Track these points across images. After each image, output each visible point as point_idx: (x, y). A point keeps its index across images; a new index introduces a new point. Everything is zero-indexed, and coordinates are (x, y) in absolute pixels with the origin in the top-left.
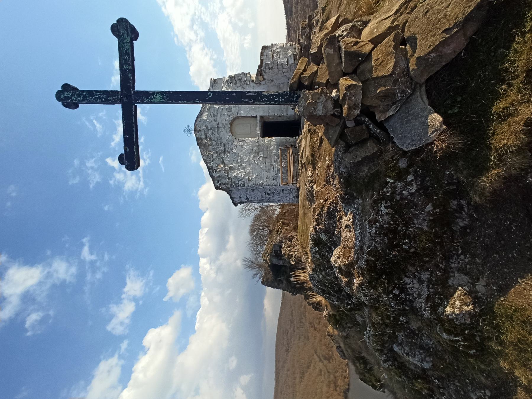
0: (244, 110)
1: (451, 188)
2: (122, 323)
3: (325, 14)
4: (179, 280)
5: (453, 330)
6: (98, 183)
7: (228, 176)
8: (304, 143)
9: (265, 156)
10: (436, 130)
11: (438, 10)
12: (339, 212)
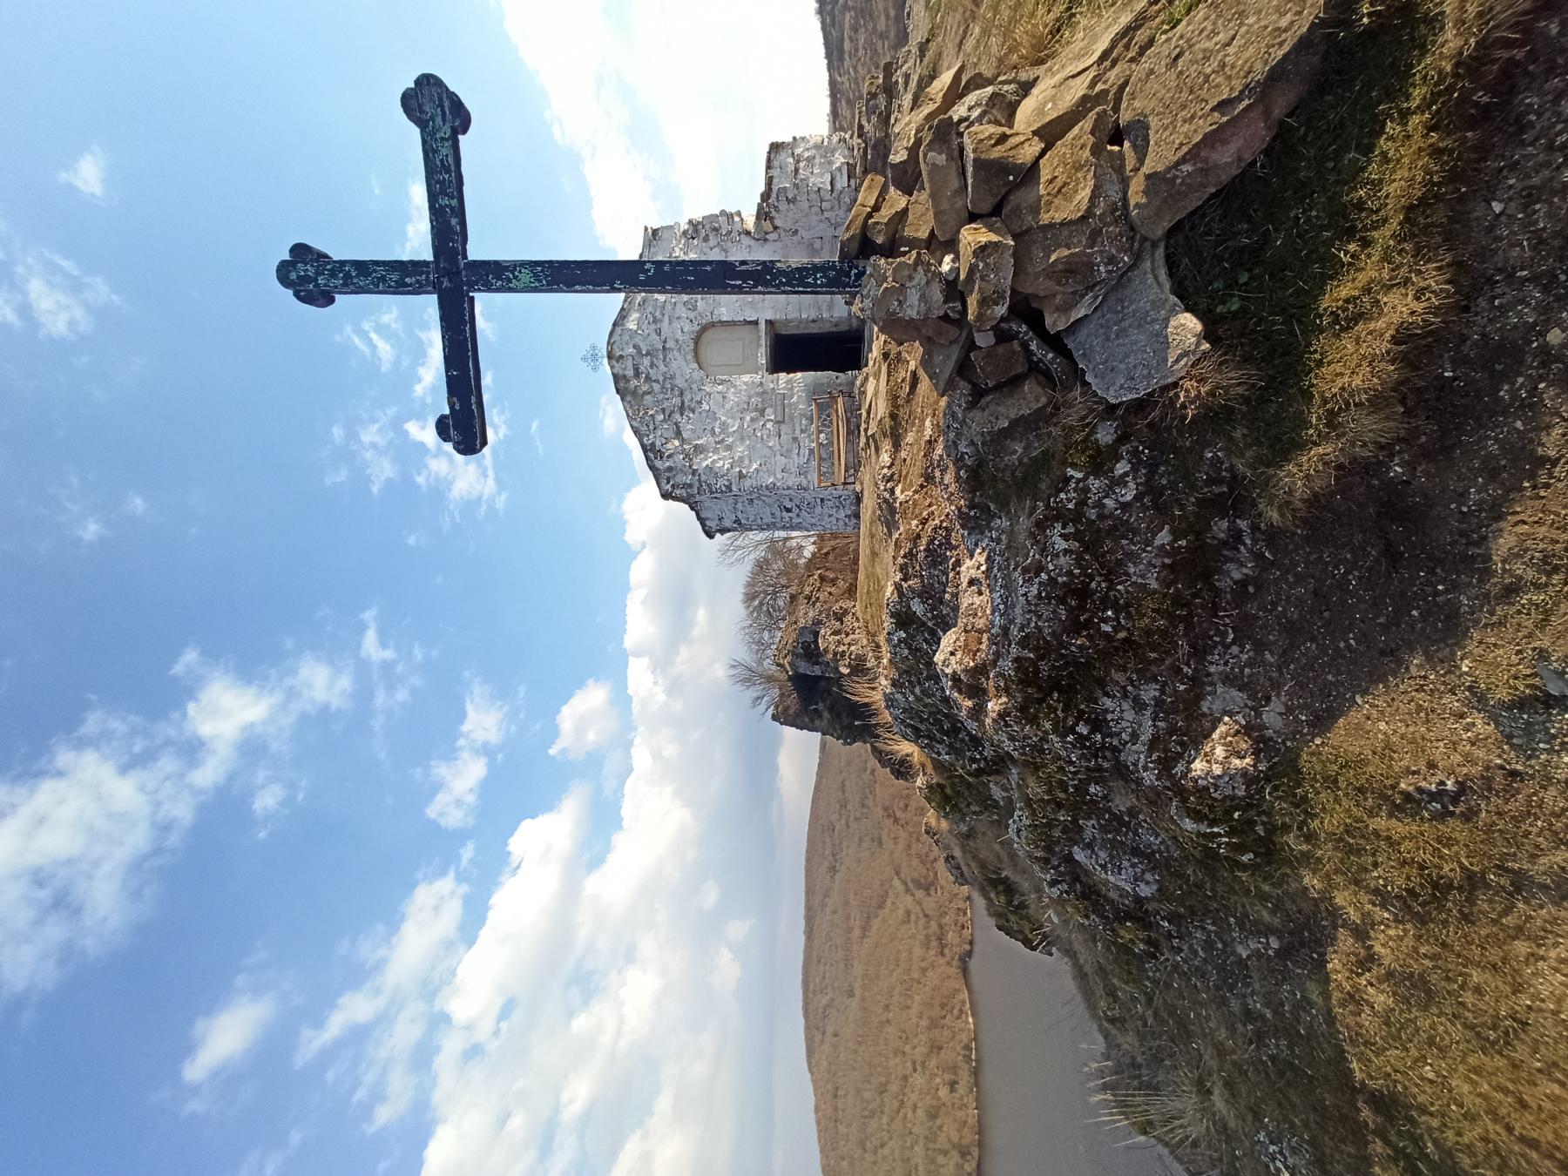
0: (727, 306)
1: (1216, 490)
2: (459, 803)
3: (926, 60)
4: (585, 707)
5: (1206, 810)
6: (389, 482)
8: (874, 386)
10: (1185, 354)
11: (1204, 50)
12: (955, 548)
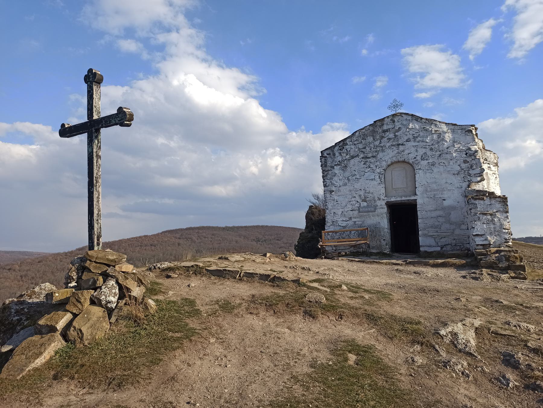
9: (361, 210)
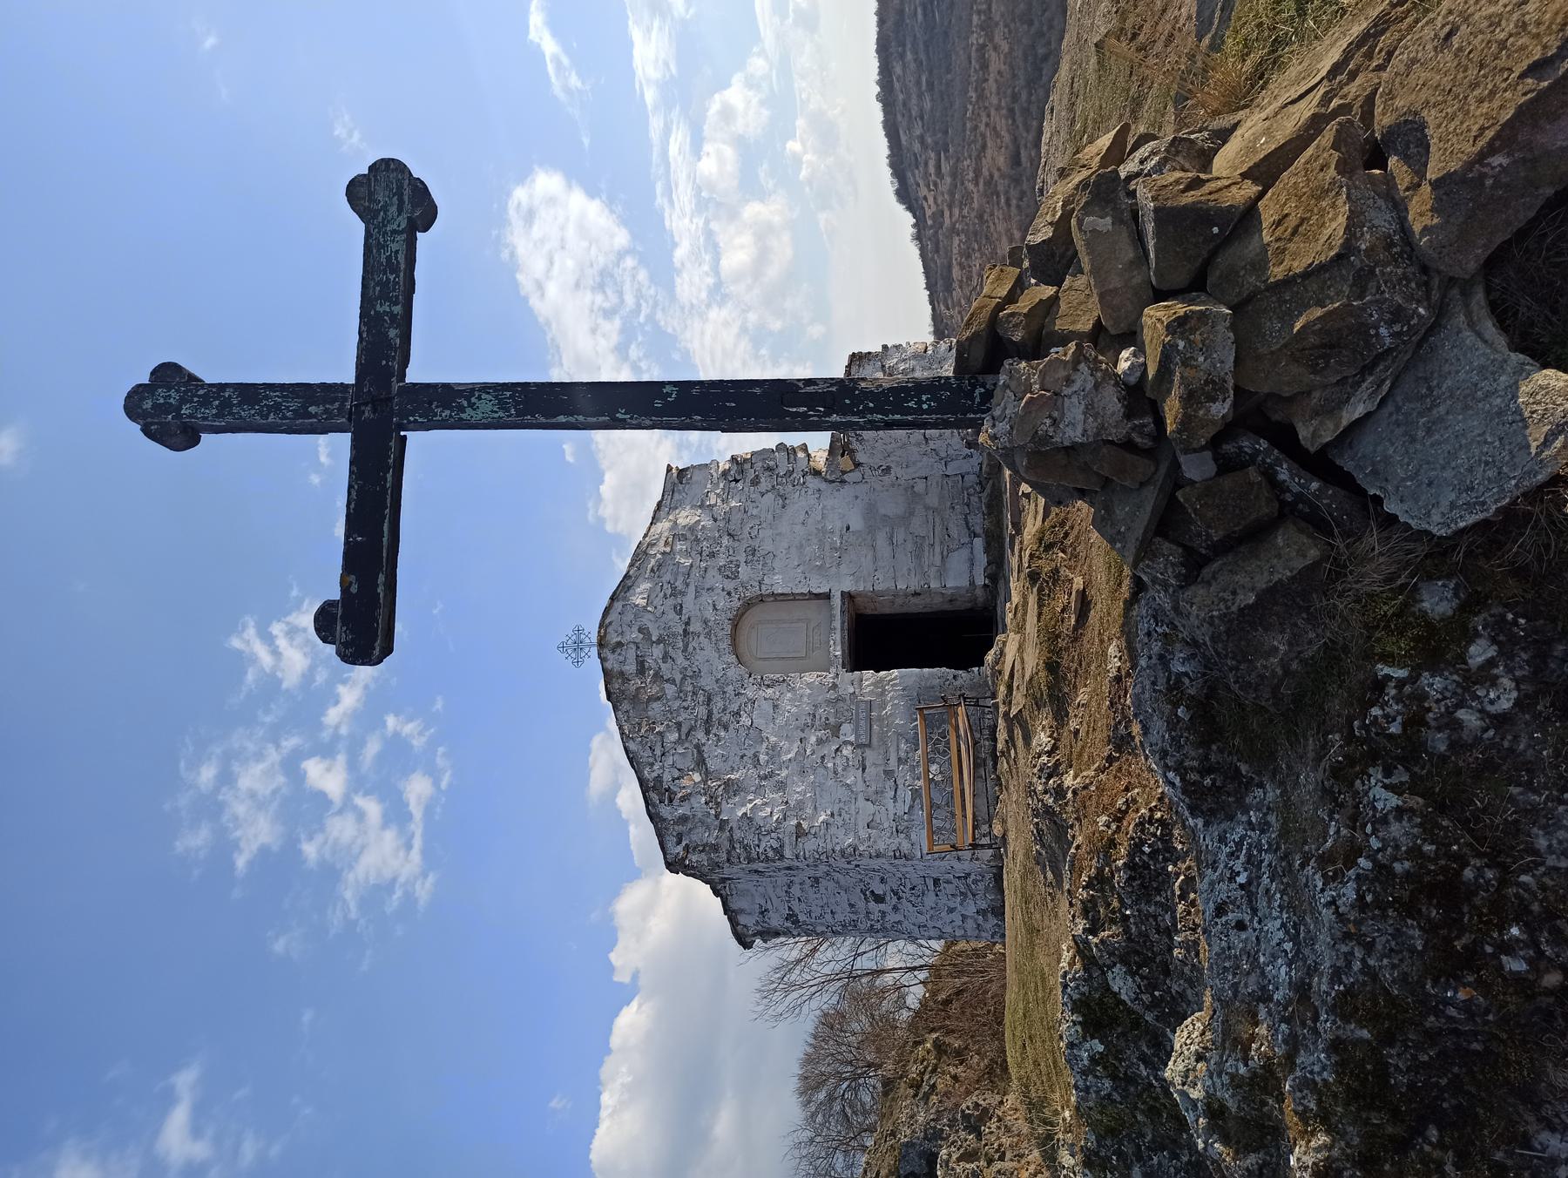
7: (717, 816)
9: (863, 740)
12: (1182, 857)
